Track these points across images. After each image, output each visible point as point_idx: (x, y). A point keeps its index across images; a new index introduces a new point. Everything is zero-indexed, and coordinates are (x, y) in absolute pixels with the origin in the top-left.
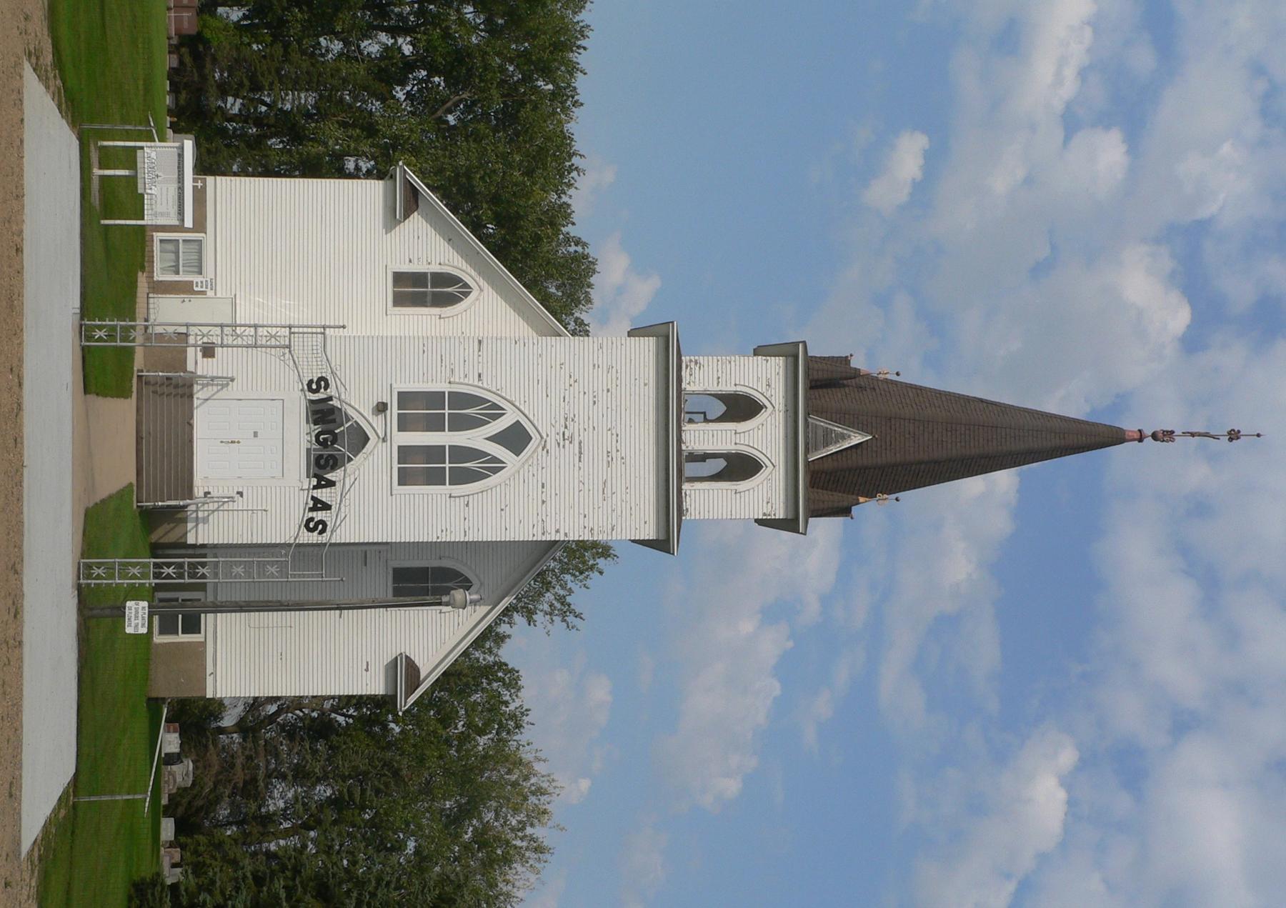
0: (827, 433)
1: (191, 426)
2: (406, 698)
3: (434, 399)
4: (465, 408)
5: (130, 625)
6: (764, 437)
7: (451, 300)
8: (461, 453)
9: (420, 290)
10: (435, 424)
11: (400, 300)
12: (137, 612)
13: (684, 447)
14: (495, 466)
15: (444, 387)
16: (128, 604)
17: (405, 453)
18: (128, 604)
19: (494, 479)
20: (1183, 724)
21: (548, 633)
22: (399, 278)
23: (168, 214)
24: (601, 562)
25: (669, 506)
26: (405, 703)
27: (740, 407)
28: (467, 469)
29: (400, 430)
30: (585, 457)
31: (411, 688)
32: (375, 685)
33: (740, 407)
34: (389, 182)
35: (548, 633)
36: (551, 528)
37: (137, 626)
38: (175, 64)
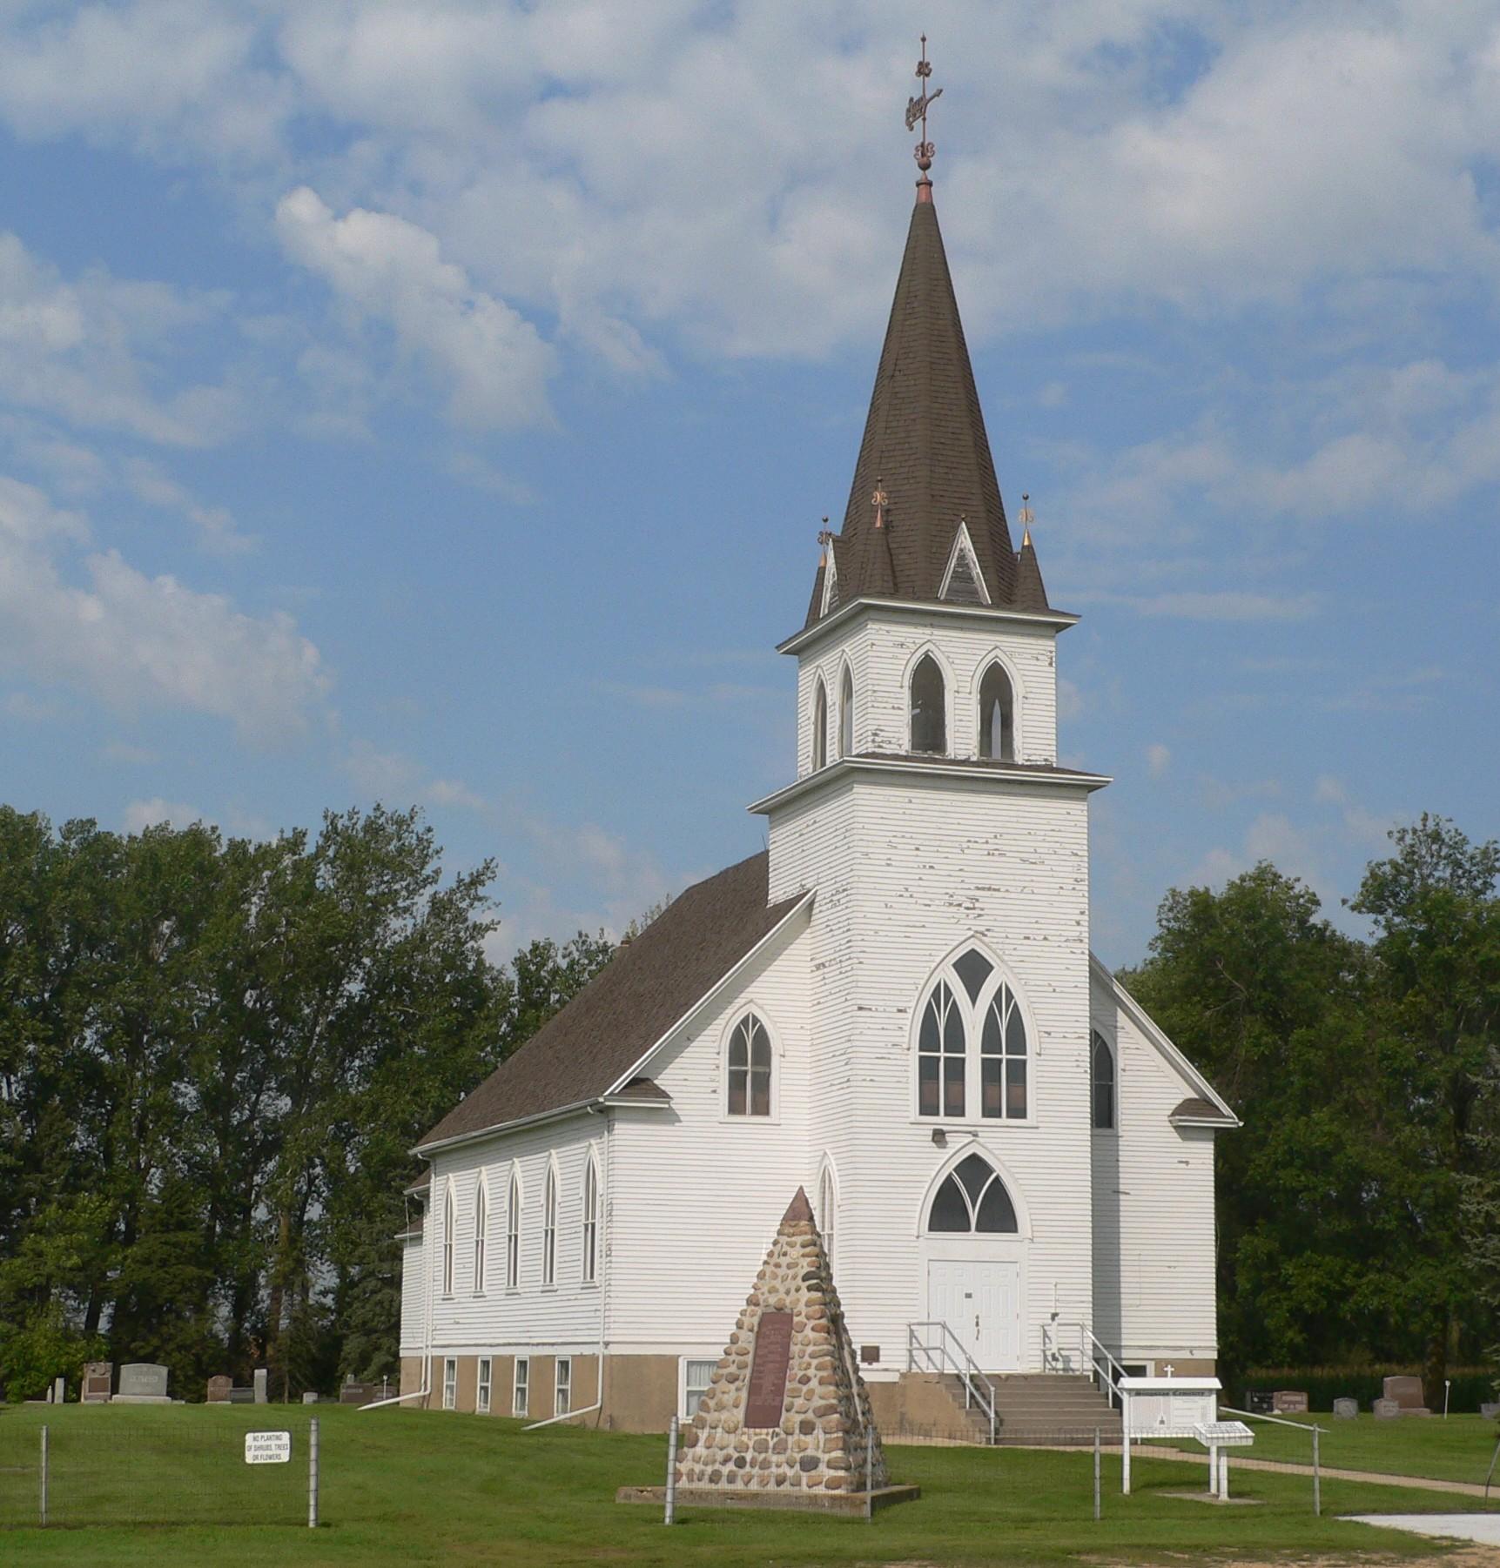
0: (956, 576)
1: (1009, 1377)
2: (1224, 1116)
3: (927, 1069)
4: (939, 1033)
5: (278, 1456)
6: (963, 657)
7: (762, 1039)
8: (990, 1041)
9: (750, 1082)
10: (956, 1070)
11: (762, 1108)
12: (260, 1448)
13: (974, 759)
14: (1004, 997)
15: (915, 1055)
16: (249, 1460)
17: (991, 1110)
18: (249, 1460)
19: (1019, 998)
20: (267, 58)
21: (497, 905)
22: (736, 1107)
23: (1204, 1408)
24: (418, 827)
25: (1047, 783)
26: (1229, 1119)
27: (927, 684)
28: (1007, 1033)
29: (962, 1114)
30: (995, 884)
31: (1214, 1110)
32: (1204, 1153)
33: (927, 684)
34: (617, 1114)
35: (497, 905)
36: (1074, 931)
37: (279, 1447)
38: (1302, 1398)
